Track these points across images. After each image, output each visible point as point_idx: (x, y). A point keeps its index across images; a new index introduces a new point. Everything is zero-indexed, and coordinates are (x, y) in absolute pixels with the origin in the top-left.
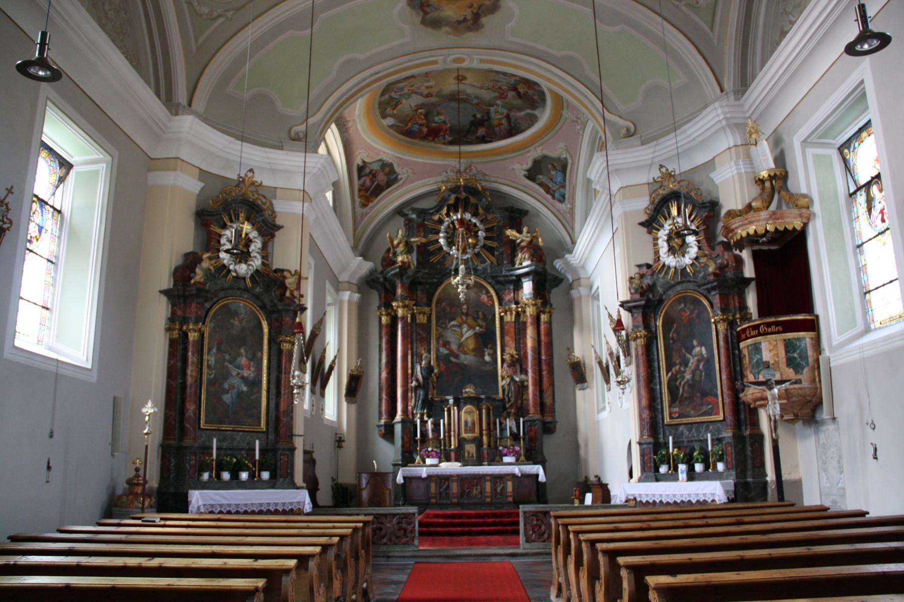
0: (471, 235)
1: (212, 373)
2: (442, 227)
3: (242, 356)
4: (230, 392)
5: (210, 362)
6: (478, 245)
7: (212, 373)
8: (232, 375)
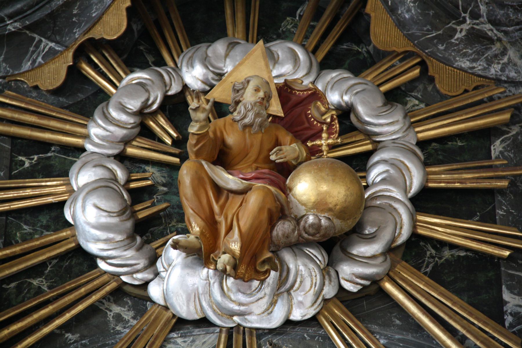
0: (315, 152)
2: (94, 131)
6: (371, 238)
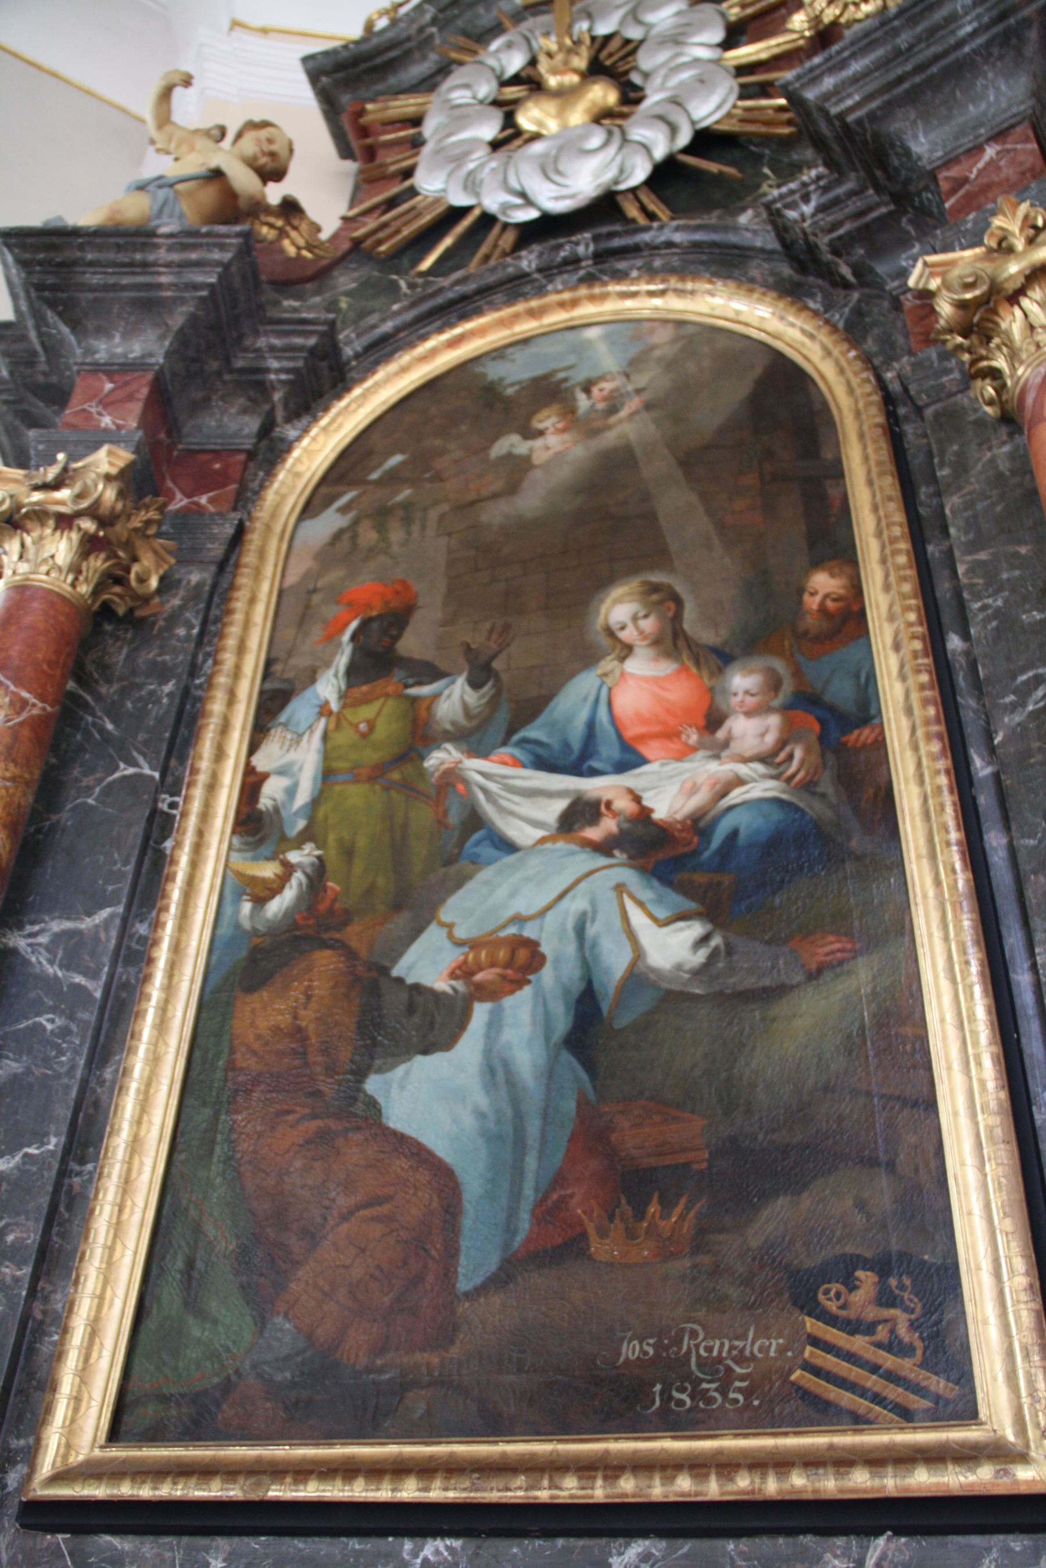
1: (289, 868)
3: (627, 650)
4: (481, 1012)
5: (271, 791)
7: (289, 868)
8: (509, 847)
